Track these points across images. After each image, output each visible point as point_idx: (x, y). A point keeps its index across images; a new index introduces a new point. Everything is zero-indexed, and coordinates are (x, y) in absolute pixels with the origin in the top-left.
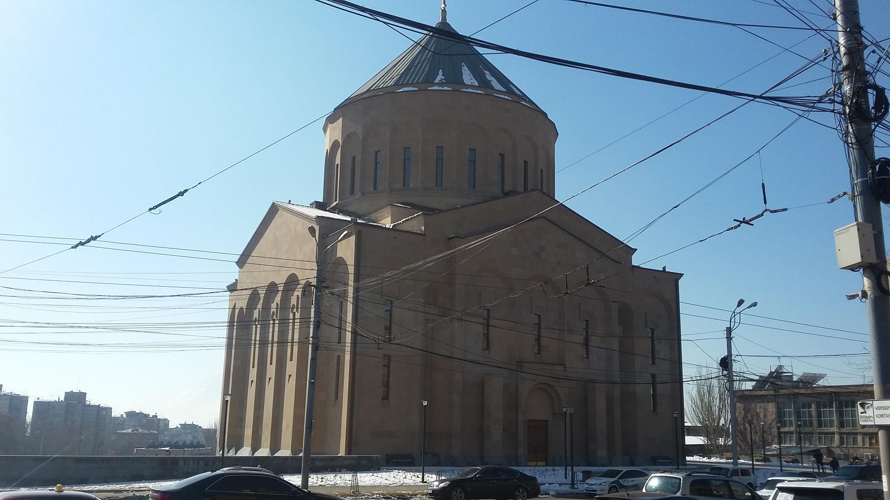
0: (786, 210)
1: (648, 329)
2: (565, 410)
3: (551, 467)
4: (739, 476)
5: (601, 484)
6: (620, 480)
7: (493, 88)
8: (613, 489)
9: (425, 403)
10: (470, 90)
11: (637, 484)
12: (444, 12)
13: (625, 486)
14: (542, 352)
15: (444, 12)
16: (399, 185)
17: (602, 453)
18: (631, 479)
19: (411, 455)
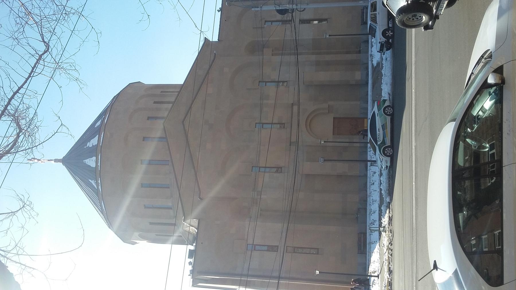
0: (49, 160)
1: (265, 26)
2: (323, 142)
3: (368, 153)
4: (376, 14)
5: (381, 162)
6: (379, 143)
7: (97, 145)
8: (386, 152)
9: (318, 273)
10: (99, 164)
11: (382, 126)
12: (56, 161)
13: (384, 140)
14: (283, 122)
15: (56, 161)
16: (171, 212)
17: (358, 76)
18: (378, 132)
19: (358, 233)
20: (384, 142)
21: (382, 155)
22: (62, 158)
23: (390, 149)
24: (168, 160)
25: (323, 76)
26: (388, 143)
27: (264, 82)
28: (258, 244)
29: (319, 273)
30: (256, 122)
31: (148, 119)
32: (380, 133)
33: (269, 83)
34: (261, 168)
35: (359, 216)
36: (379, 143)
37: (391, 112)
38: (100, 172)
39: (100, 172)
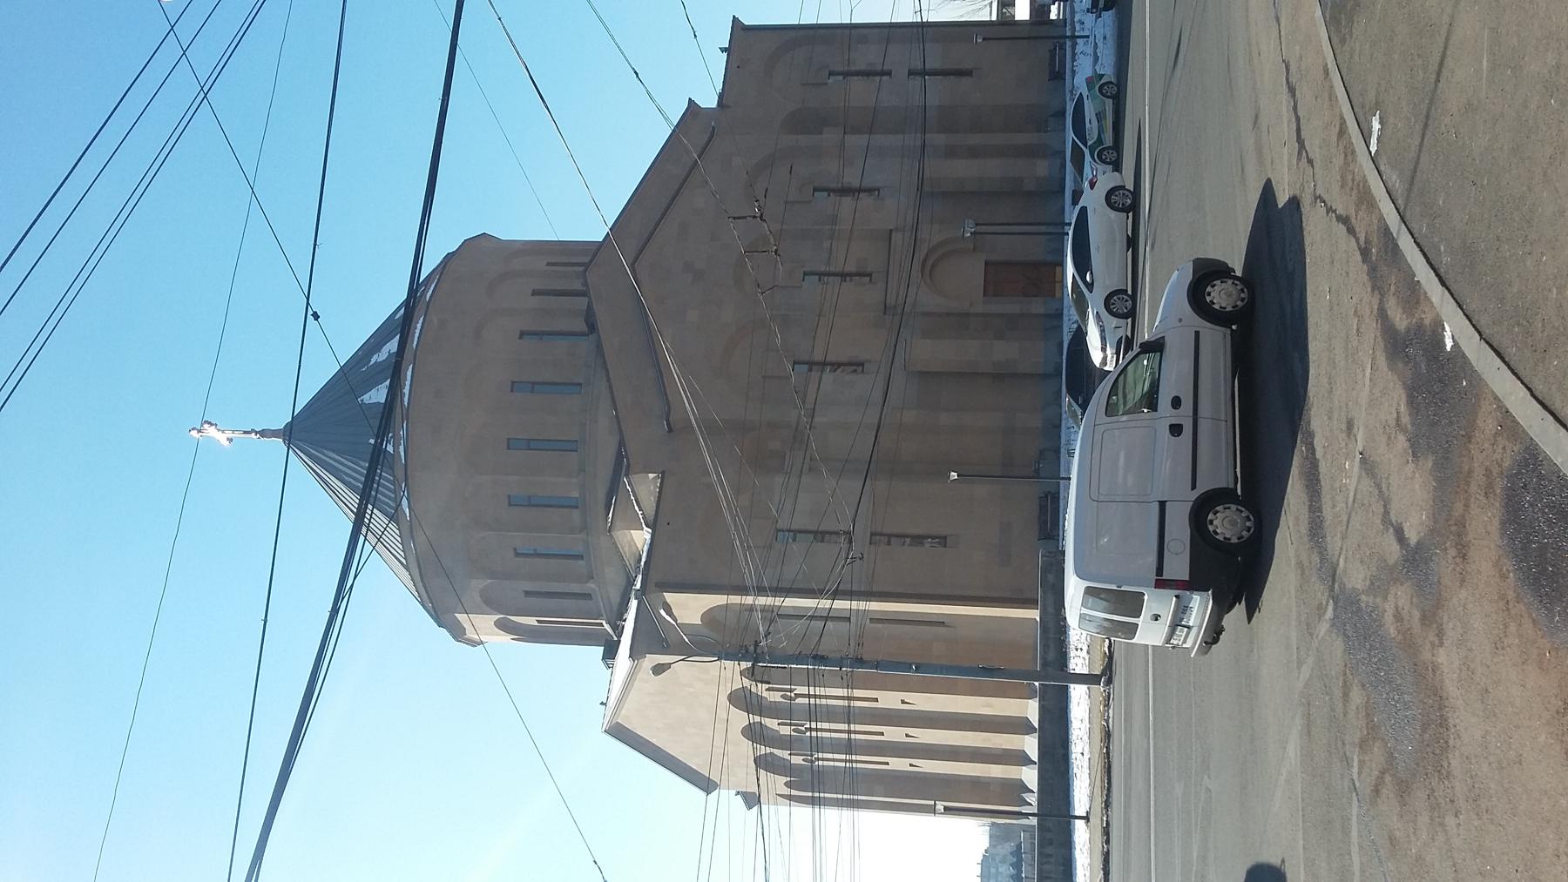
1: (829, 81)
2: (969, 235)
6: (1089, 143)
8: (1104, 92)
12: (263, 433)
14: (869, 270)
15: (263, 433)
17: (1042, 168)
20: (1100, 141)
21: (1095, 161)
22: (282, 428)
23: (1111, 151)
24: (581, 381)
25: (963, 170)
26: (1108, 140)
27: (792, 531)
28: (803, 528)
29: (956, 477)
30: (805, 269)
31: (533, 295)
32: (1091, 126)
33: (802, 535)
34: (798, 535)
35: (1041, 466)
36: (1089, 143)
37: (1113, 159)
38: (428, 307)
39: (428, 307)
